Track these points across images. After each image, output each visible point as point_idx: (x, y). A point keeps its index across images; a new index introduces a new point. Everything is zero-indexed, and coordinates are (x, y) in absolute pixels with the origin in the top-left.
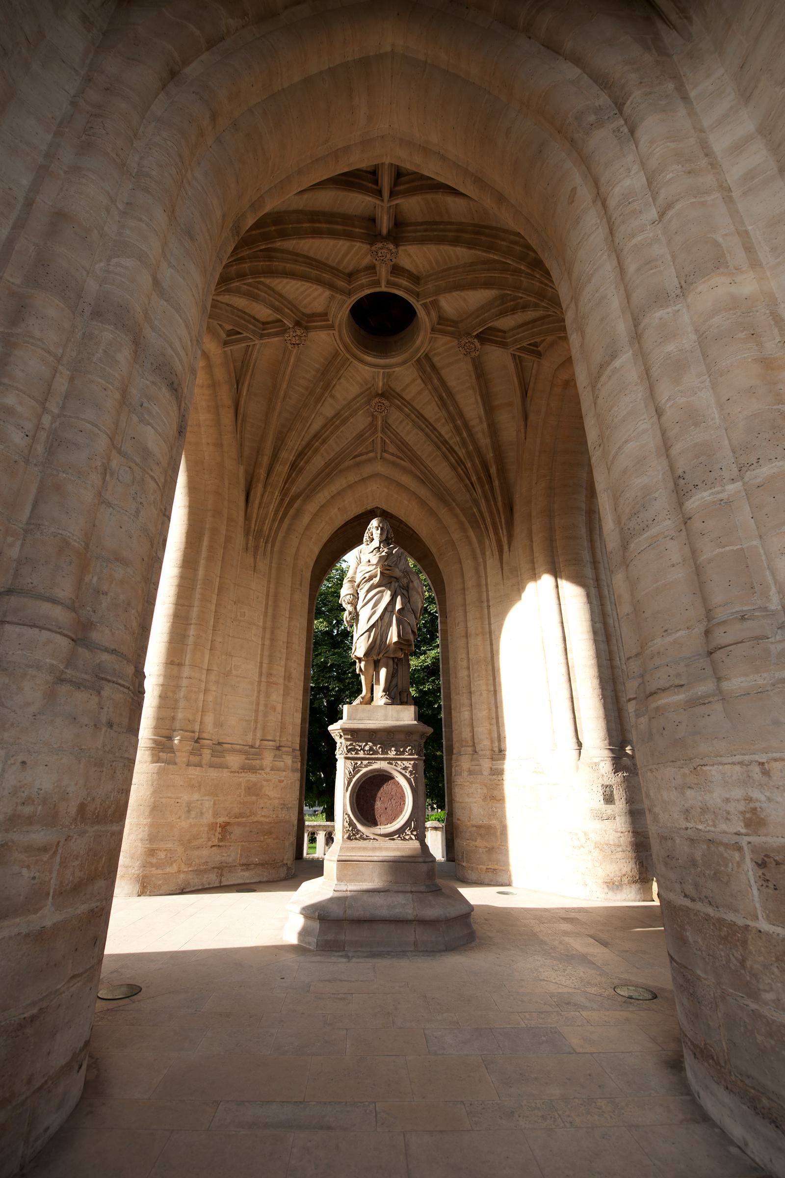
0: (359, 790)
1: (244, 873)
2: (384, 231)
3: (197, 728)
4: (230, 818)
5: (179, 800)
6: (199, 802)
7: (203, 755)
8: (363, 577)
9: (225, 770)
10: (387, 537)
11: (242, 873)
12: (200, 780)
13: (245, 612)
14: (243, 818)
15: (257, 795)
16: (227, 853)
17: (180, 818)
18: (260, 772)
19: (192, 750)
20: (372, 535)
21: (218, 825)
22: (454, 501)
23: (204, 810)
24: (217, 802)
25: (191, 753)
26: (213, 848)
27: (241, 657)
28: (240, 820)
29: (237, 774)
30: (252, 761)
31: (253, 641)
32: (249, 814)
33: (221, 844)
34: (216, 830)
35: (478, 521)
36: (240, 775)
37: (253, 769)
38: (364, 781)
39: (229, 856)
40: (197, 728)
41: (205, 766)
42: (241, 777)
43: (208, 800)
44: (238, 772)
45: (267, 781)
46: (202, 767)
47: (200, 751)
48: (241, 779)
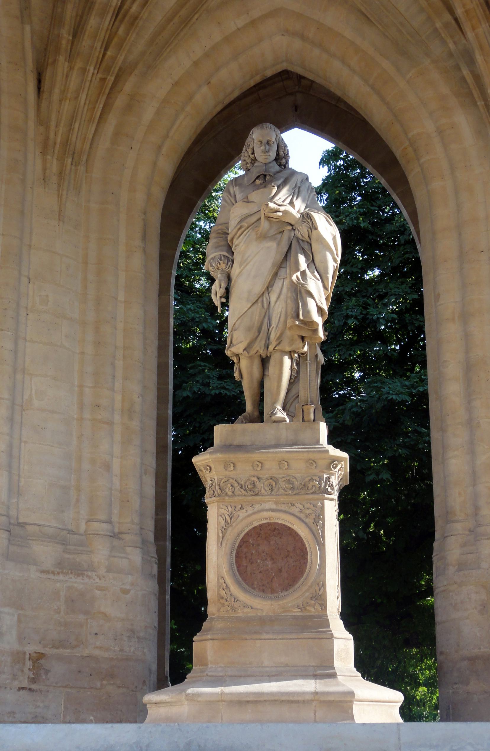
0: (240, 546)
8: (239, 226)
10: (278, 155)
13: (47, 296)
14: (66, 648)
18: (89, 574)
20: (253, 153)
21: (27, 656)
26: (22, 692)
29: (51, 576)
33: (33, 687)
34: (24, 664)
36: (56, 577)
38: (247, 534)
44: (53, 573)
48: (58, 585)
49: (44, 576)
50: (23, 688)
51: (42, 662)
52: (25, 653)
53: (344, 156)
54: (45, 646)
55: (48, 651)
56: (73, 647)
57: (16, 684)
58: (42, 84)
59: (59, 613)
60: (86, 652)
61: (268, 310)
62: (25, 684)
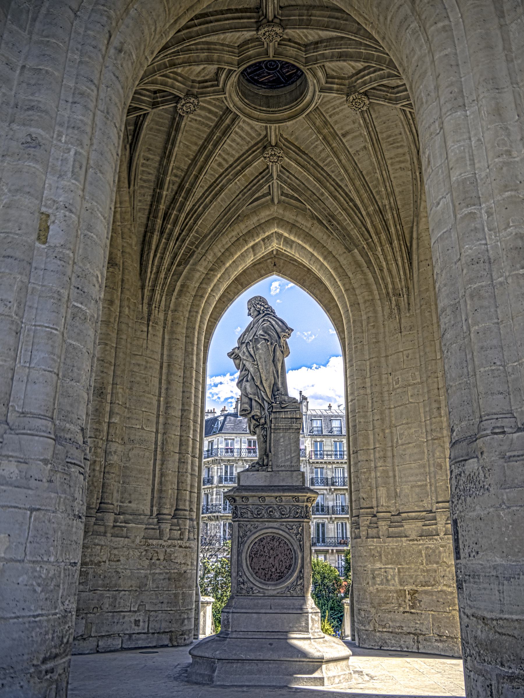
1: (439, 644)
2: (270, 16)
3: (374, 504)
4: (417, 586)
5: (365, 569)
6: (383, 570)
7: (380, 527)
9: (404, 539)
11: (436, 644)
12: (379, 550)
14: (429, 586)
15: (437, 563)
16: (419, 620)
17: (368, 583)
18: (436, 537)
19: (370, 523)
21: (407, 592)
22: (203, 312)
23: (390, 577)
24: (401, 570)
25: (369, 527)
26: (406, 614)
27: (402, 424)
28: (426, 588)
29: (416, 542)
30: (429, 527)
31: (411, 403)
32: (433, 583)
33: (412, 611)
34: (405, 597)
35: (318, 259)
36: (419, 543)
37: (430, 535)
39: (422, 623)
40: (374, 504)
41: (381, 537)
42: (420, 545)
43: (391, 568)
44: (417, 540)
45: (442, 546)
46: (379, 538)
47: (376, 524)
48: (420, 547)
49: (411, 543)
50: (406, 612)
51: (416, 595)
52: (405, 591)
53: (468, 244)
54: (417, 586)
55: (420, 589)
56: (433, 586)
57: (401, 609)
58: (141, 239)
59: (423, 564)
60: (440, 588)
61: (409, 245)
62: (408, 609)
